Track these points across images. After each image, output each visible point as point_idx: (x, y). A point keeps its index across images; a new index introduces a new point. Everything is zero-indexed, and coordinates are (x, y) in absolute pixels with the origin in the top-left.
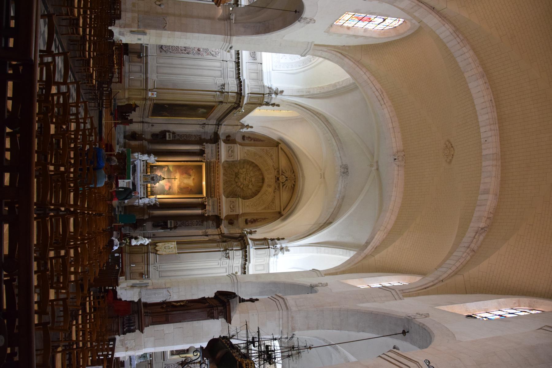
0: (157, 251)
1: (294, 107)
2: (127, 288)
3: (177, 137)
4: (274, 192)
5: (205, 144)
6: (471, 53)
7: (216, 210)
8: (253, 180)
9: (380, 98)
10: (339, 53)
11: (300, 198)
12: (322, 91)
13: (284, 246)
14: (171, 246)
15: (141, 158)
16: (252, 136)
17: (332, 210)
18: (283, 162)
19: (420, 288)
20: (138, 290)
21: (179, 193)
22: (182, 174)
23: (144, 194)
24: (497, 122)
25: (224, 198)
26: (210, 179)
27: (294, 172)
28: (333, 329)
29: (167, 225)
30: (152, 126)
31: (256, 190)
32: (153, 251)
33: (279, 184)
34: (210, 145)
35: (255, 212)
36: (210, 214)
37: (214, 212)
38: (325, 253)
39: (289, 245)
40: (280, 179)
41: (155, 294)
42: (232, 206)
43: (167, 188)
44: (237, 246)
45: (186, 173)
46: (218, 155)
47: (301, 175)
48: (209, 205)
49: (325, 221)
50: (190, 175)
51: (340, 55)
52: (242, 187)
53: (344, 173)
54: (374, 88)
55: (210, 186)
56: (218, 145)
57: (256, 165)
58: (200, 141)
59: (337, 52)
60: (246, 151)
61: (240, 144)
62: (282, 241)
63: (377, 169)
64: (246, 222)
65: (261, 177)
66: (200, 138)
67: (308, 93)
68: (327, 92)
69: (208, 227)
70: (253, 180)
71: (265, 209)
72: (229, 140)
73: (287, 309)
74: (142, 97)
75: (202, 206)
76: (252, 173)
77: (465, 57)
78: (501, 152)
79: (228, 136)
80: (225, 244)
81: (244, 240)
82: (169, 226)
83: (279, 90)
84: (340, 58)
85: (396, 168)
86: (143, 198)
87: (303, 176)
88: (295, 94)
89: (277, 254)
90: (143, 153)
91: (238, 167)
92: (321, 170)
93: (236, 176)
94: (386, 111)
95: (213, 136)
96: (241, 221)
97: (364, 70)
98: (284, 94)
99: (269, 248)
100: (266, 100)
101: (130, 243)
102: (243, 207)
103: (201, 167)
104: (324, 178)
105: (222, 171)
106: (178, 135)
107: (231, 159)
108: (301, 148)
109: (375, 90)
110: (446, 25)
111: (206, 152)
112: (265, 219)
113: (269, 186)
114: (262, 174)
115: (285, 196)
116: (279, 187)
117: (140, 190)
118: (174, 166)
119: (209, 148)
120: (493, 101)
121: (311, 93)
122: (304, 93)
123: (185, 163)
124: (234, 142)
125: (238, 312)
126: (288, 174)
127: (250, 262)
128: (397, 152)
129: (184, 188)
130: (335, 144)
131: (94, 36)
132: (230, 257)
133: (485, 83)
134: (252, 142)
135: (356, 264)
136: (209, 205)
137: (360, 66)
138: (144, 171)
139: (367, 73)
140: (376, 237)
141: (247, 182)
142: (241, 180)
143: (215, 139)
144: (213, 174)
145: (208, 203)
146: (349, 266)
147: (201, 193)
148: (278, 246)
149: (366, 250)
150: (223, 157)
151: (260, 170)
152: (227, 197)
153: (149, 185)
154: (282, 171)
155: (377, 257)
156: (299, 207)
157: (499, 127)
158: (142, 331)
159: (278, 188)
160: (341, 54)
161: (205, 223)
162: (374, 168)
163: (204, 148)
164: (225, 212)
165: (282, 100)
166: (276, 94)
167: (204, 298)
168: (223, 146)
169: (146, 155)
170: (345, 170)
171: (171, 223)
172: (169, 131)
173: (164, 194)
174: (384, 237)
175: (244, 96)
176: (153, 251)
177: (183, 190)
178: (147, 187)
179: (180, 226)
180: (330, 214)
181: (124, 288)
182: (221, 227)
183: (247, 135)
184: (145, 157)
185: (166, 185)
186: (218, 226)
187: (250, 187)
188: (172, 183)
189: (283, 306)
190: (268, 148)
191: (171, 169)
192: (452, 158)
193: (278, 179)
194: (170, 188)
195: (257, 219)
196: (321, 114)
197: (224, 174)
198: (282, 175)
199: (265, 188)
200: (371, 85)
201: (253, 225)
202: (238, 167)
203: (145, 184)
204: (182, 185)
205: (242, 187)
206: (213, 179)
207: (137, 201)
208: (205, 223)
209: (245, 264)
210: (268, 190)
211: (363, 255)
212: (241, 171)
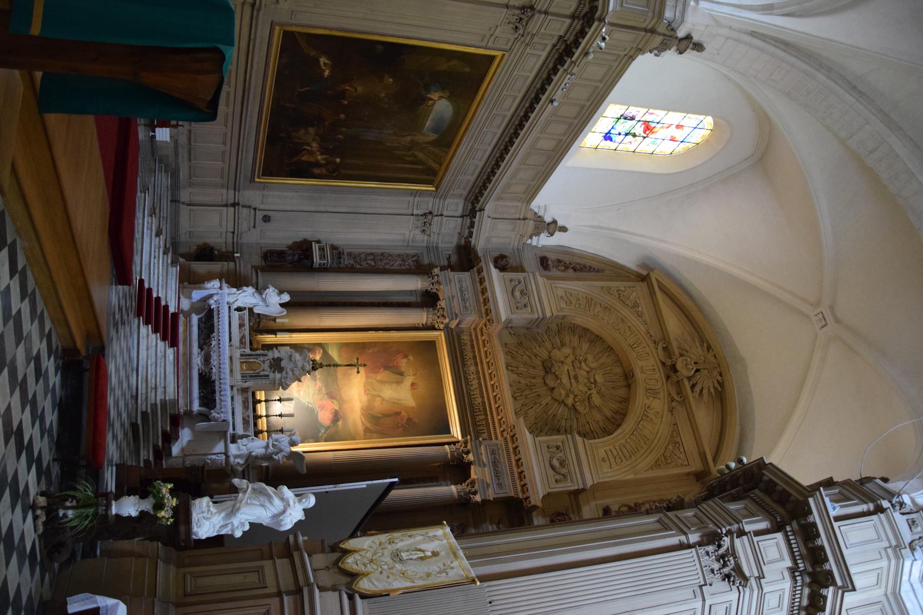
3: (346, 261)
4: (671, 410)
7: (507, 481)
8: (599, 379)
14: (429, 547)
16: (567, 259)
18: (673, 323)
30: (267, 219)
31: (616, 412)
32: (326, 578)
35: (631, 477)
36: (491, 495)
37: (500, 485)
40: (679, 366)
42: (556, 463)
43: (325, 417)
45: (387, 367)
50: (402, 374)
52: (570, 401)
55: (471, 405)
56: (480, 271)
60: (560, 293)
65: (618, 370)
66: (417, 261)
71: (657, 465)
75: (458, 469)
76: (590, 358)
79: (502, 257)
91: (548, 345)
101: (183, 515)
103: (431, 345)
106: (350, 254)
113: (651, 392)
115: (705, 418)
117: (229, 407)
118: (344, 346)
119: (453, 287)
123: (381, 334)
124: (520, 269)
126: (696, 352)
129: (386, 415)
138: (242, 342)
141: (582, 388)
142: (565, 380)
145: (478, 455)
154: (679, 348)
164: (539, 485)
165: (713, 18)
169: (250, 290)
173: (317, 440)
177: (382, 422)
183: (552, 257)
184: (246, 297)
185: (322, 407)
187: (596, 400)
188: (341, 402)
193: (674, 368)
194: (336, 417)
197: (508, 366)
198: (682, 355)
199: (640, 399)
204: (378, 406)
205: (570, 401)
206: (475, 382)
207: (220, 447)
212: (557, 354)
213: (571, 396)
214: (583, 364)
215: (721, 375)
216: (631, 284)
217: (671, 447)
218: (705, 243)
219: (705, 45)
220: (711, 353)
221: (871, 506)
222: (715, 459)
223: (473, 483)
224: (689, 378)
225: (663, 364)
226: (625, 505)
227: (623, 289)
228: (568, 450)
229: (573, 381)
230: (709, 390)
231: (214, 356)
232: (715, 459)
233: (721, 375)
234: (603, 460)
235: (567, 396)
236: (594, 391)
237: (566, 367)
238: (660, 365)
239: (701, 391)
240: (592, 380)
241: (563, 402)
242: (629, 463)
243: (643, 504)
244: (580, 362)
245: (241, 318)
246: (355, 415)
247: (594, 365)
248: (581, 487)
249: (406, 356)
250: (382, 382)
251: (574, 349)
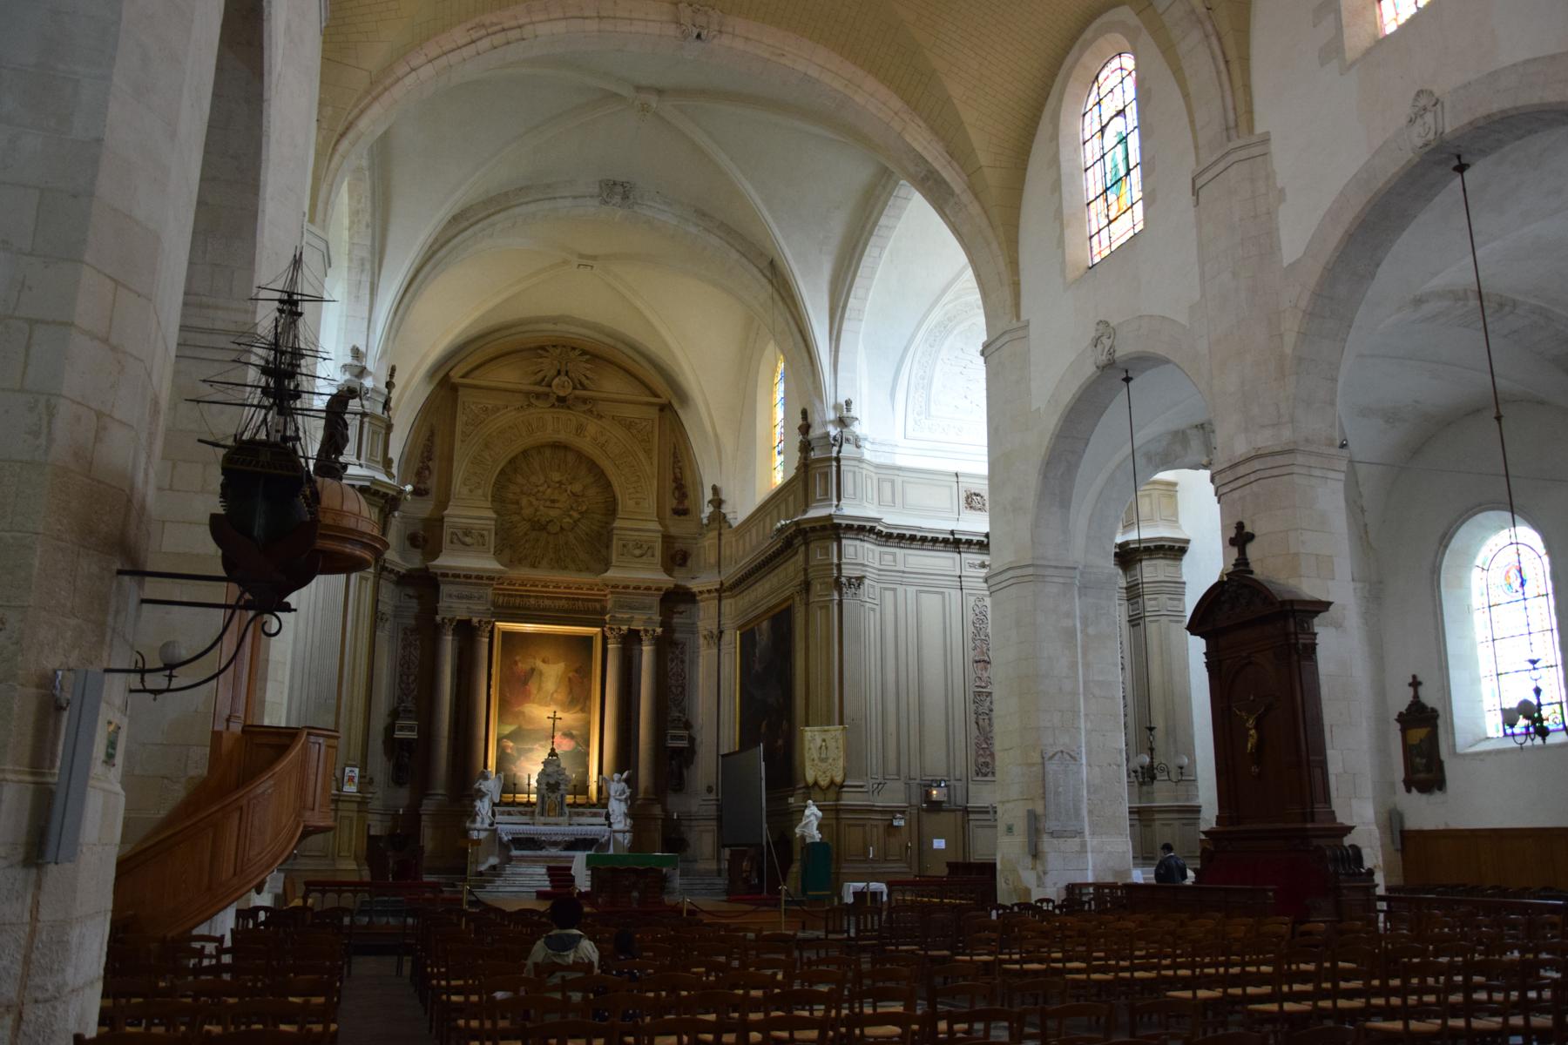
0: (832, 783)
1: (402, 320)
2: (1040, 868)
4: (600, 417)
5: (438, 618)
8: (556, 476)
9: (499, 39)
10: (338, 142)
11: (612, 334)
12: (367, 217)
13: (831, 415)
15: (487, 821)
18: (509, 376)
19: (1224, 77)
20: (1046, 838)
21: (585, 709)
22: (525, 696)
23: (595, 815)
25: (609, 574)
26: (544, 610)
27: (543, 348)
28: (1345, 340)
29: (681, 750)
33: (577, 398)
34: (443, 603)
36: (657, 618)
37: (650, 608)
38: (866, 299)
39: (830, 401)
40: (562, 394)
41: (1057, 794)
42: (637, 552)
44: (827, 552)
45: (525, 683)
46: (467, 577)
47: (550, 327)
48: (631, 620)
49: (764, 281)
50: (533, 670)
51: (345, 144)
52: (576, 515)
53: (625, 197)
54: (466, 52)
55: (566, 611)
56: (446, 575)
57: (512, 461)
58: (425, 630)
59: (334, 149)
60: (465, 490)
61: (443, 504)
62: (815, 419)
63: (660, 92)
64: (681, 512)
67: (368, 266)
68: (373, 202)
69: (692, 629)
70: (556, 476)
71: (648, 452)
72: (426, 538)
73: (1291, 451)
74: (355, 815)
75: (630, 640)
80: (817, 587)
81: (813, 529)
82: (684, 744)
83: (349, 360)
84: (353, 144)
85: (726, 40)
86: (608, 817)
88: (366, 309)
89: (857, 439)
90: (472, 815)
91: (516, 518)
93: (543, 528)
94: (544, 29)
95: (411, 592)
96: (678, 528)
98: (362, 348)
99: (838, 460)
100: (379, 410)
102: (640, 517)
103: (508, 636)
104: (594, 258)
105: (523, 572)
106: (401, 700)
107: (491, 540)
108: (476, 314)
109: (472, 49)
111: (465, 617)
113: (580, 430)
114: (539, 448)
115: (612, 385)
116: (585, 401)
117: (589, 826)
118: (501, 720)
119: (453, 605)
122: (366, 278)
125: (1292, 582)
127: (878, 520)
128: (678, 23)
129: (571, 691)
130: (532, 208)
131: (1131, 957)
132: (858, 574)
134: (434, 465)
135: (991, 224)
136: (631, 620)
137: (388, 82)
139: (414, 64)
140: (919, 149)
142: (553, 513)
143: (424, 584)
144: (532, 601)
145: (623, 621)
146: (995, 246)
147: (587, 641)
148: (833, 431)
149: (952, 185)
150: (483, 562)
151: (525, 453)
152: (607, 565)
153: (569, 799)
154: (539, 384)
155: (984, 158)
156: (652, 347)
158: (1349, 829)
159: (589, 404)
160: (342, 135)
161: (677, 636)
162: (653, 101)
163: (451, 620)
164: (653, 575)
167: (1208, 665)
168: (448, 560)
169: (478, 804)
170: (618, 191)
171: (674, 738)
172: (390, 729)
173: (587, 754)
175: (374, 481)
176: (831, 794)
177: (577, 695)
178: (574, 805)
179: (683, 711)
180: (744, 260)
181: (1039, 878)
182: (695, 590)
186: (689, 597)
187: (577, 488)
189: (1280, 460)
191: (508, 729)
193: (562, 400)
195: (676, 480)
197: (533, 566)
199: (585, 445)
200: (453, 58)
201: (691, 494)
202: (516, 518)
203: (567, 810)
204: (562, 696)
205: (576, 515)
206: (548, 602)
208: (677, 636)
209: (879, 534)
210: (591, 435)
211: (966, 198)
212: (527, 512)
215: (574, 349)
218: (449, 317)
222: (657, 396)
223: (646, 631)
224: (575, 388)
231: (554, 838)
233: (574, 349)
245: (502, 813)
246: (569, 718)
247: (542, 479)
249: (516, 663)
250: (540, 689)
251: (522, 493)
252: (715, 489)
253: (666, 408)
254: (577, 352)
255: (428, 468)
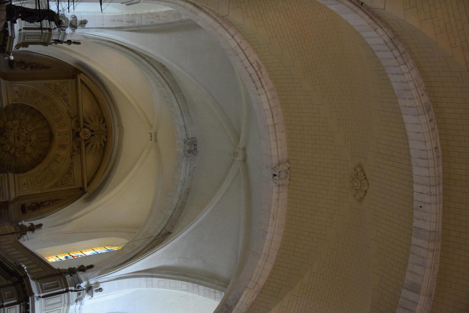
4: (72, 156)
6: (415, 73)
8: (33, 138)
9: (255, 77)
12: (156, 21)
13: (92, 282)
17: (170, 213)
18: (86, 105)
24: (441, 182)
27: (104, 121)
33: (80, 142)
38: (159, 287)
40: (81, 134)
44: (10, 297)
47: (116, 123)
49: (159, 231)
52: (12, 151)
53: (189, 152)
54: (246, 62)
57: (39, 112)
62: (89, 273)
67: (131, 24)
77: (403, 77)
78: (443, 228)
81: (23, 286)
83: (79, 19)
84: (191, 10)
85: (275, 189)
87: (120, 125)
92: (151, 126)
94: (264, 98)
97: (232, 31)
98: (87, 26)
99: (67, 291)
104: (156, 140)
109: (248, 64)
110: (380, 30)
112: (56, 200)
113: (63, 147)
115: (90, 161)
116: (79, 147)
120: (439, 149)
121: (137, 23)
122: (124, 24)
128: (279, 164)
130: (176, 105)
133: (430, 121)
137: (225, 25)
139: (236, 37)
148: (83, 285)
154: (85, 121)
157: (444, 190)
162: (240, 158)
166: (74, 27)
170: (192, 147)
174: (254, 299)
175: (13, 38)
187: (29, 150)
190: (58, 82)
192: (365, 195)
193: (78, 135)
196: (151, 58)
198: (84, 127)
200: (242, 56)
213: (13, 149)
214: (25, 130)
215: (106, 137)
216: (65, 81)
217: (66, 176)
219: (87, 20)
220: (104, 125)
221: (65, 290)
222: (88, 185)
224: (85, 140)
225: (73, 130)
226: (34, 203)
227: (58, 84)
228: (4, 182)
229: (16, 140)
230: (96, 146)
232: (88, 185)
233: (106, 137)
234: (25, 184)
235: (11, 148)
236: (28, 145)
237: (14, 132)
238: (71, 130)
239: (92, 147)
240: (28, 139)
241: (8, 151)
242: (39, 185)
243: (45, 202)
244: (23, 129)
248: (8, 200)
252: (40, 226)
253: (82, 191)
254: (105, 139)
255: (26, 67)
